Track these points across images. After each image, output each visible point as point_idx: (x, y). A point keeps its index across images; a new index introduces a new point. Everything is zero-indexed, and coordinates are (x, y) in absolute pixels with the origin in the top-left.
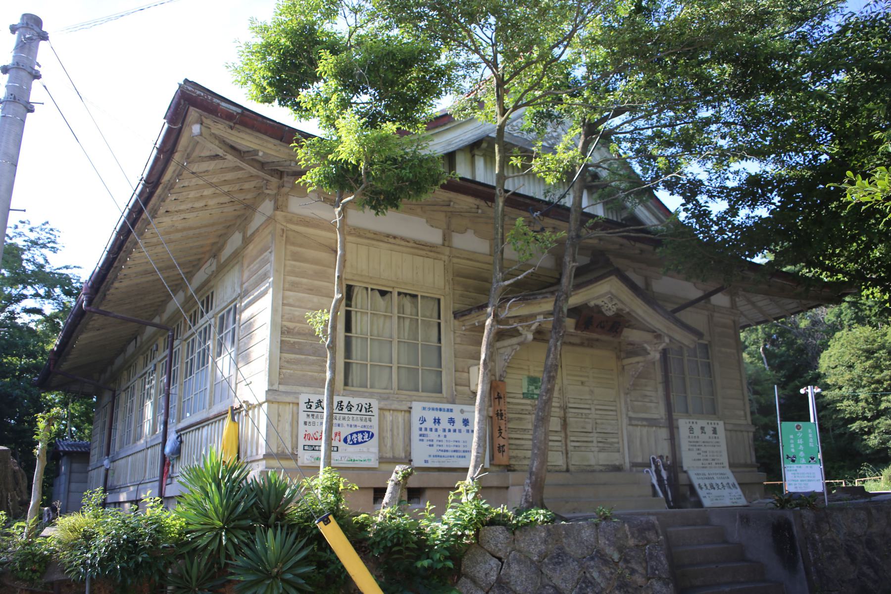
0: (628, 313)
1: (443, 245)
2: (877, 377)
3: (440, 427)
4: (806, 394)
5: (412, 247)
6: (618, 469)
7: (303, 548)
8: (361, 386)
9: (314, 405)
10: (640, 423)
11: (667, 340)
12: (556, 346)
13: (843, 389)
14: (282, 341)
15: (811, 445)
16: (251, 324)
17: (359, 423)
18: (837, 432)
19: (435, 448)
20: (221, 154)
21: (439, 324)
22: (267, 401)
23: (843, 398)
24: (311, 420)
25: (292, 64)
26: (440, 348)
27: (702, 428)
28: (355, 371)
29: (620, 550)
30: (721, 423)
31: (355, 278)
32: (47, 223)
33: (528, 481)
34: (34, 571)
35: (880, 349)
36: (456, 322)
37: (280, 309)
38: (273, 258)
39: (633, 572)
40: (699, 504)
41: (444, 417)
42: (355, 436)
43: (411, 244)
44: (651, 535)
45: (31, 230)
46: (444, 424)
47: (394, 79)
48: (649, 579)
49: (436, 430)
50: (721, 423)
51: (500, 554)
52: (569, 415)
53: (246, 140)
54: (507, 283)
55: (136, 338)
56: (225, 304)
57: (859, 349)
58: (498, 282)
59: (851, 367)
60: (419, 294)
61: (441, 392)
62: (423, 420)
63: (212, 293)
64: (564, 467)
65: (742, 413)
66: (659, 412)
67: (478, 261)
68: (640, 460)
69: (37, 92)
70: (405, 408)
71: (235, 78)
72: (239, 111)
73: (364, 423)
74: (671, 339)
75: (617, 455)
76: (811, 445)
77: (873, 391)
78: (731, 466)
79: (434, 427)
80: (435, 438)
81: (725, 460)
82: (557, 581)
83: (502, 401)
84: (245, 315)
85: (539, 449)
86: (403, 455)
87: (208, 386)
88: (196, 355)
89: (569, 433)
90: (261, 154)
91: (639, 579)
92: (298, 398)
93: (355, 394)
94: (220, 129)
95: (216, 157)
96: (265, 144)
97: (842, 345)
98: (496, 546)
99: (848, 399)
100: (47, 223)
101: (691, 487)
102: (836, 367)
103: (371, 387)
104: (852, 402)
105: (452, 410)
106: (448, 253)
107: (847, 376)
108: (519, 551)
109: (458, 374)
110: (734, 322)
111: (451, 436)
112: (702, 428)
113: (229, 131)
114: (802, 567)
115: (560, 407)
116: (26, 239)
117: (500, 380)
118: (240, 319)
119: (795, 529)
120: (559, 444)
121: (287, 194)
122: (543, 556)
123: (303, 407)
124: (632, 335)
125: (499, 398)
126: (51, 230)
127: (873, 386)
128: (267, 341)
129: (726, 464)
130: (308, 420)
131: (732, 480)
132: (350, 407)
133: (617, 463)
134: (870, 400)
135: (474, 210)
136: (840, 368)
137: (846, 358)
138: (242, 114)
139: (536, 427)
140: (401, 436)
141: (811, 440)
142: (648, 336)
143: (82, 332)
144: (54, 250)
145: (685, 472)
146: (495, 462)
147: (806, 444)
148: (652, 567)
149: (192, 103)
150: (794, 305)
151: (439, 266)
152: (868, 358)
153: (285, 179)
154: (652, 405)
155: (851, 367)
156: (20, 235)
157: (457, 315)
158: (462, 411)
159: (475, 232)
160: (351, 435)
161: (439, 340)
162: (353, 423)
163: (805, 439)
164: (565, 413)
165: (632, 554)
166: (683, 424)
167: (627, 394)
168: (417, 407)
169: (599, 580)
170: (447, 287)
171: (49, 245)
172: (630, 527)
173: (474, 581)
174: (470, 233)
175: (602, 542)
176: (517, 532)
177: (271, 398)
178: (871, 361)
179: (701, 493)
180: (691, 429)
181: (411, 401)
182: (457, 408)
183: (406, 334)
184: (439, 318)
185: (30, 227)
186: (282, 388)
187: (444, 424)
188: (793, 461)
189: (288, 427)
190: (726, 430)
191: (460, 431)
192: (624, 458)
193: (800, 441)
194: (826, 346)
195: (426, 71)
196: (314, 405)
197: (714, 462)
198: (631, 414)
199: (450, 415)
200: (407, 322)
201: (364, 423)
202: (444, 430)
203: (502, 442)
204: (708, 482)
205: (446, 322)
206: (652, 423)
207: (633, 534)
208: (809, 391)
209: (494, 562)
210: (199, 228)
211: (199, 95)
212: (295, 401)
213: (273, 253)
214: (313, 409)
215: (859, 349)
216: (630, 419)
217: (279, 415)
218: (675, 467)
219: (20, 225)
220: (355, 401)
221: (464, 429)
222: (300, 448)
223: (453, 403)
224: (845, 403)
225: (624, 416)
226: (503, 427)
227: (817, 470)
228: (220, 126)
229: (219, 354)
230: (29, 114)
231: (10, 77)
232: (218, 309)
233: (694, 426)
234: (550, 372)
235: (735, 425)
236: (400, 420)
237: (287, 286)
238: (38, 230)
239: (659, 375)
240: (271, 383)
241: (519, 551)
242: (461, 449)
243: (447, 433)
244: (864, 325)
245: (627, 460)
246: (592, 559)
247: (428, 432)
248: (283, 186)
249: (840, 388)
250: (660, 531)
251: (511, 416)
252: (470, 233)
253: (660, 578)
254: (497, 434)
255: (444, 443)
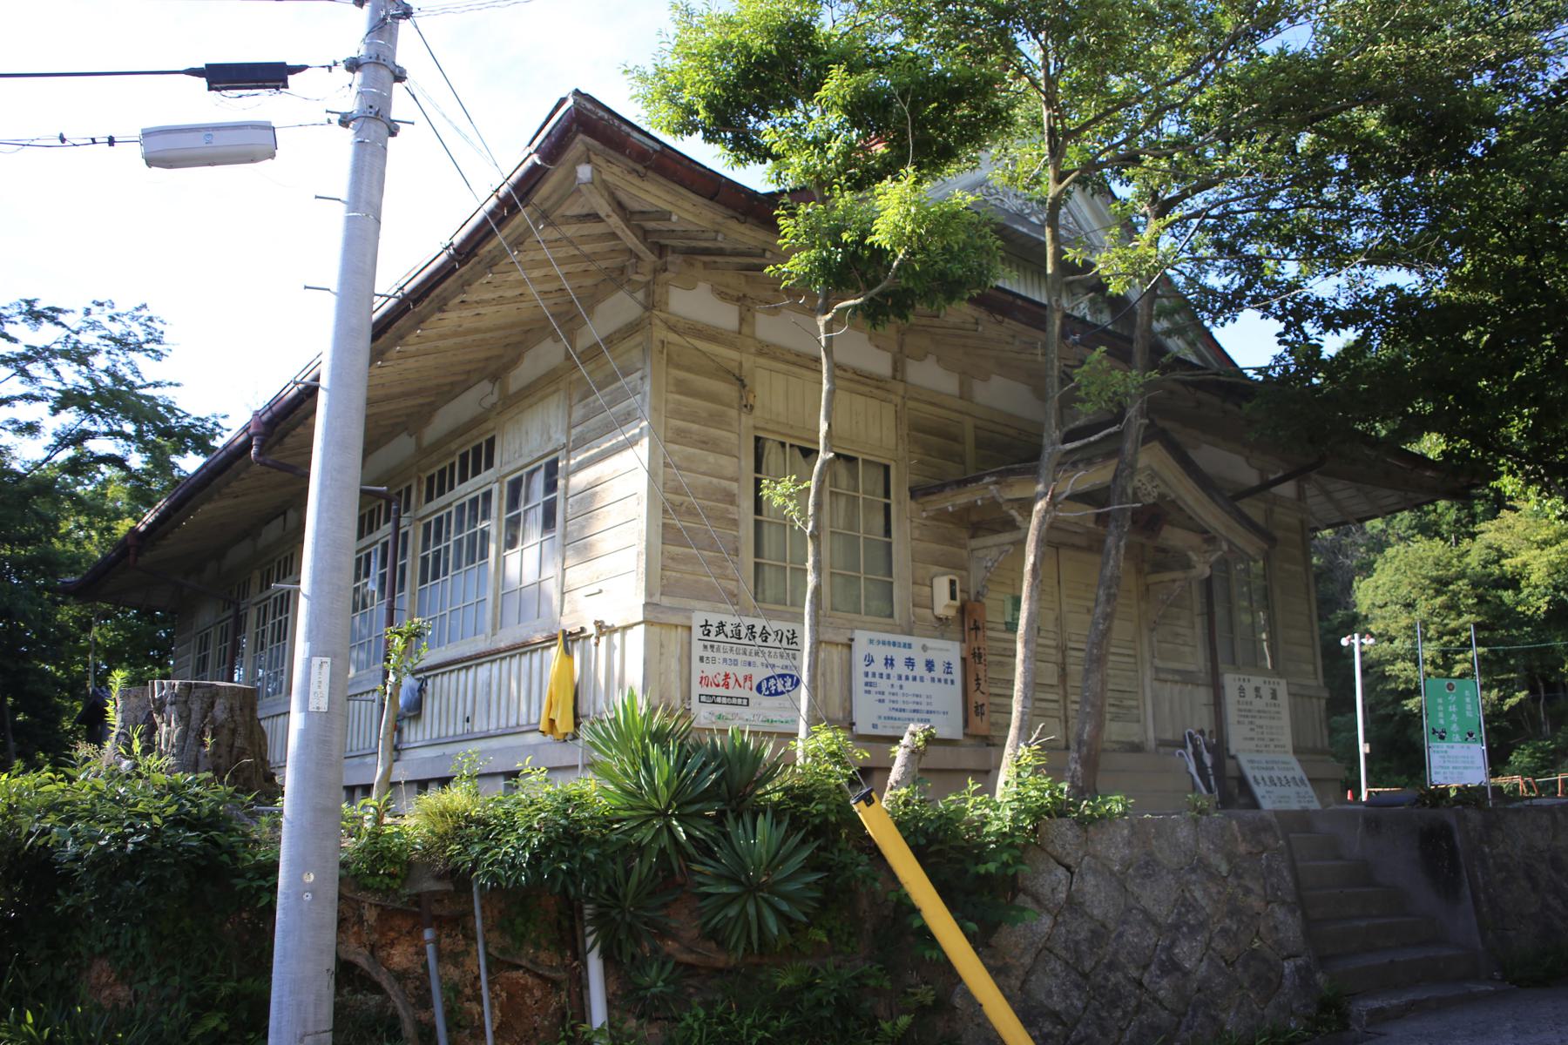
0: (1173, 501)
1: (894, 378)
2: (1453, 624)
3: (894, 672)
4: (1351, 646)
5: (851, 380)
6: (1136, 748)
7: (797, 848)
8: (777, 602)
9: (713, 630)
10: (1170, 677)
11: (1225, 547)
12: (1118, 547)
13: (1396, 643)
14: (664, 525)
15: (1469, 714)
16: (594, 494)
17: (779, 662)
18: (1382, 712)
19: (887, 705)
20: (602, 215)
21: (887, 508)
22: (645, 622)
23: (1396, 657)
24: (709, 654)
25: (758, 80)
26: (889, 545)
27: (1257, 689)
28: (769, 575)
29: (1230, 857)
30: (1283, 682)
31: (769, 426)
32: (145, 306)
33: (1075, 755)
34: (392, 876)
35: (1458, 579)
36: (914, 505)
37: (661, 472)
38: (647, 388)
39: (1248, 891)
40: (1254, 804)
41: (900, 655)
42: (772, 681)
43: (849, 375)
44: (1268, 839)
45: (112, 319)
46: (900, 667)
47: (924, 119)
48: (1268, 903)
49: (888, 676)
50: (1283, 682)
51: (1068, 861)
52: (1070, 660)
53: (651, 194)
54: (1069, 446)
55: (284, 513)
56: (529, 459)
57: (1425, 577)
58: (1053, 444)
59: (1410, 606)
60: (860, 457)
61: (891, 616)
62: (870, 660)
63: (491, 443)
64: (1063, 743)
65: (1310, 668)
66: (1196, 661)
67: (943, 407)
68: (1168, 736)
69: (400, 105)
70: (845, 641)
71: (634, 92)
72: (658, 147)
73: (787, 663)
74: (1230, 543)
75: (1135, 727)
76: (1469, 714)
77: (1444, 645)
78: (1297, 751)
79: (885, 672)
80: (888, 690)
81: (1287, 739)
82: (1147, 902)
83: (980, 633)
84: (580, 480)
85: (1093, 706)
86: (840, 715)
87: (490, 597)
88: (451, 543)
89: (1069, 690)
90: (674, 218)
91: (1256, 903)
92: (689, 618)
93: (770, 615)
94: (617, 174)
95: (594, 217)
96: (680, 203)
97: (1397, 569)
98: (1063, 847)
99: (1404, 660)
100: (145, 306)
101: (1242, 781)
102: (1386, 605)
103: (792, 605)
104: (1409, 665)
105: (910, 646)
106: (901, 392)
107: (1404, 620)
108: (1095, 857)
109: (917, 588)
110: (1302, 522)
111: (910, 687)
112: (1257, 689)
113: (636, 181)
114: (1468, 892)
115: (1056, 647)
116: (103, 333)
117: (977, 600)
118: (566, 487)
119: (1458, 838)
120: (1055, 705)
121: (667, 284)
122: (1127, 864)
123: (697, 632)
124: (1174, 537)
125: (977, 628)
126: (151, 319)
127: (1445, 638)
128: (641, 525)
129: (1290, 748)
130: (705, 654)
131: (1298, 772)
132: (765, 635)
133: (1136, 739)
134: (1440, 661)
135: (968, 326)
136: (1391, 608)
137: (1404, 591)
138: (662, 153)
139: (1087, 671)
140: (837, 683)
141: (1469, 707)
142: (1195, 539)
143: (209, 499)
144: (159, 356)
145: (1233, 757)
146: (969, 731)
147: (1461, 712)
148: (1272, 886)
149: (584, 126)
150: (1392, 500)
151: (889, 411)
152: (1438, 593)
153: (670, 258)
154: (1187, 649)
155: (1410, 606)
156: (94, 325)
157: (916, 493)
158: (925, 648)
159: (938, 360)
160: (768, 679)
161: (888, 532)
162: (771, 661)
163: (1460, 704)
164: (1064, 657)
165: (1246, 865)
166: (1230, 681)
167: (1152, 630)
168: (861, 637)
169: (1203, 903)
170: (900, 448)
171: (146, 346)
172: (1240, 826)
173: (1037, 900)
174: (931, 360)
175: (1205, 846)
176: (1091, 828)
177: (650, 617)
178: (1444, 598)
179: (1259, 791)
180: (1241, 690)
181: (852, 630)
182: (917, 642)
183: (841, 522)
184: (887, 494)
185: (112, 312)
186: (666, 601)
187: (900, 667)
188: (1442, 738)
189: (674, 665)
190: (1290, 694)
191: (922, 679)
192: (1146, 732)
193: (1452, 708)
194: (1367, 569)
195: (977, 108)
196: (713, 630)
197: (1272, 744)
198: (1158, 663)
199: (907, 653)
200: (842, 502)
201: (787, 663)
202: (900, 677)
203: (978, 698)
204: (1266, 774)
205: (899, 503)
206: (1187, 678)
207: (1244, 835)
208: (1356, 641)
209: (1061, 873)
210: (491, 330)
211: (602, 118)
212: (686, 622)
213: (648, 382)
214: (712, 636)
215: (1425, 577)
216: (1157, 670)
217: (662, 646)
218: (1220, 749)
219: (95, 309)
220: (774, 625)
221: (927, 675)
222: (695, 698)
223: (910, 634)
224: (1400, 665)
225: (1148, 665)
226: (981, 676)
227: (1477, 753)
228: (615, 169)
229: (511, 543)
230: (391, 140)
231: (365, 78)
232: (507, 469)
233: (1245, 685)
234: (1109, 587)
235: (1302, 686)
236: (836, 658)
237: (670, 434)
238: (126, 319)
239: (1197, 603)
240: (649, 592)
241: (1095, 857)
242: (924, 707)
243: (903, 682)
244: (1431, 538)
245: (1151, 734)
246: (1193, 870)
247: (877, 679)
248: (665, 270)
249: (1391, 640)
250: (1279, 833)
251: (990, 658)
252: (931, 360)
253: (1283, 903)
254: (972, 686)
255: (900, 698)
